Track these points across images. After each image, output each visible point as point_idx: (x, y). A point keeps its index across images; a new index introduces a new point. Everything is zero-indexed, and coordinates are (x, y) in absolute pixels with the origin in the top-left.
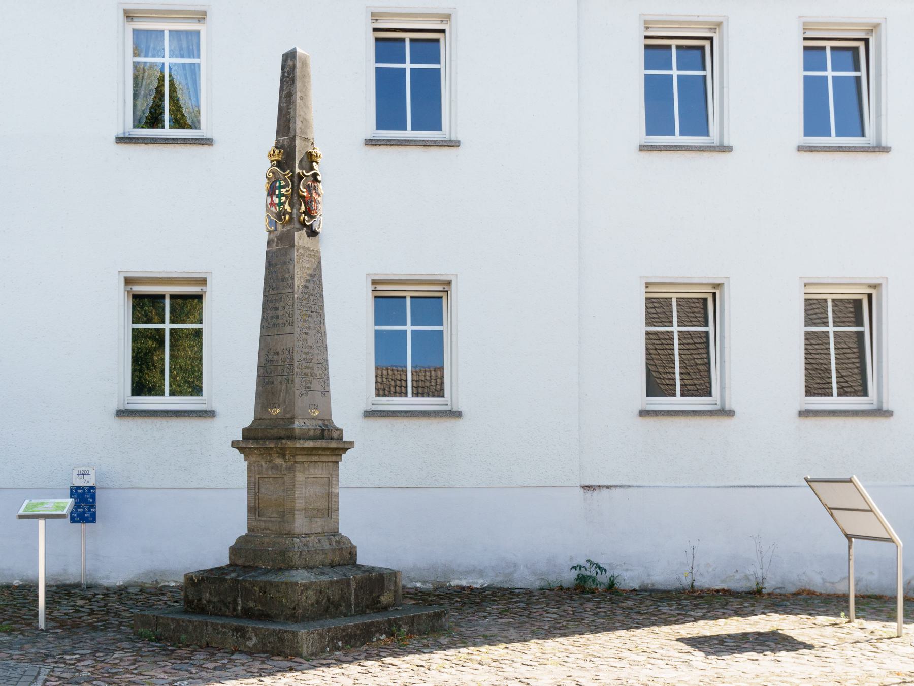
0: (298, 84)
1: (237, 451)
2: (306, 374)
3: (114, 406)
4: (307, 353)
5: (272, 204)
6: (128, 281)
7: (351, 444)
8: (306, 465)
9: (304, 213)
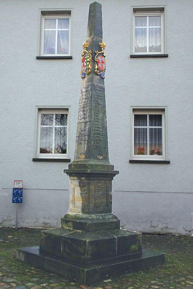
0: (150, 134)
1: (66, 174)
3: (33, 156)
4: (98, 130)
7: (117, 172)
9: (97, 69)
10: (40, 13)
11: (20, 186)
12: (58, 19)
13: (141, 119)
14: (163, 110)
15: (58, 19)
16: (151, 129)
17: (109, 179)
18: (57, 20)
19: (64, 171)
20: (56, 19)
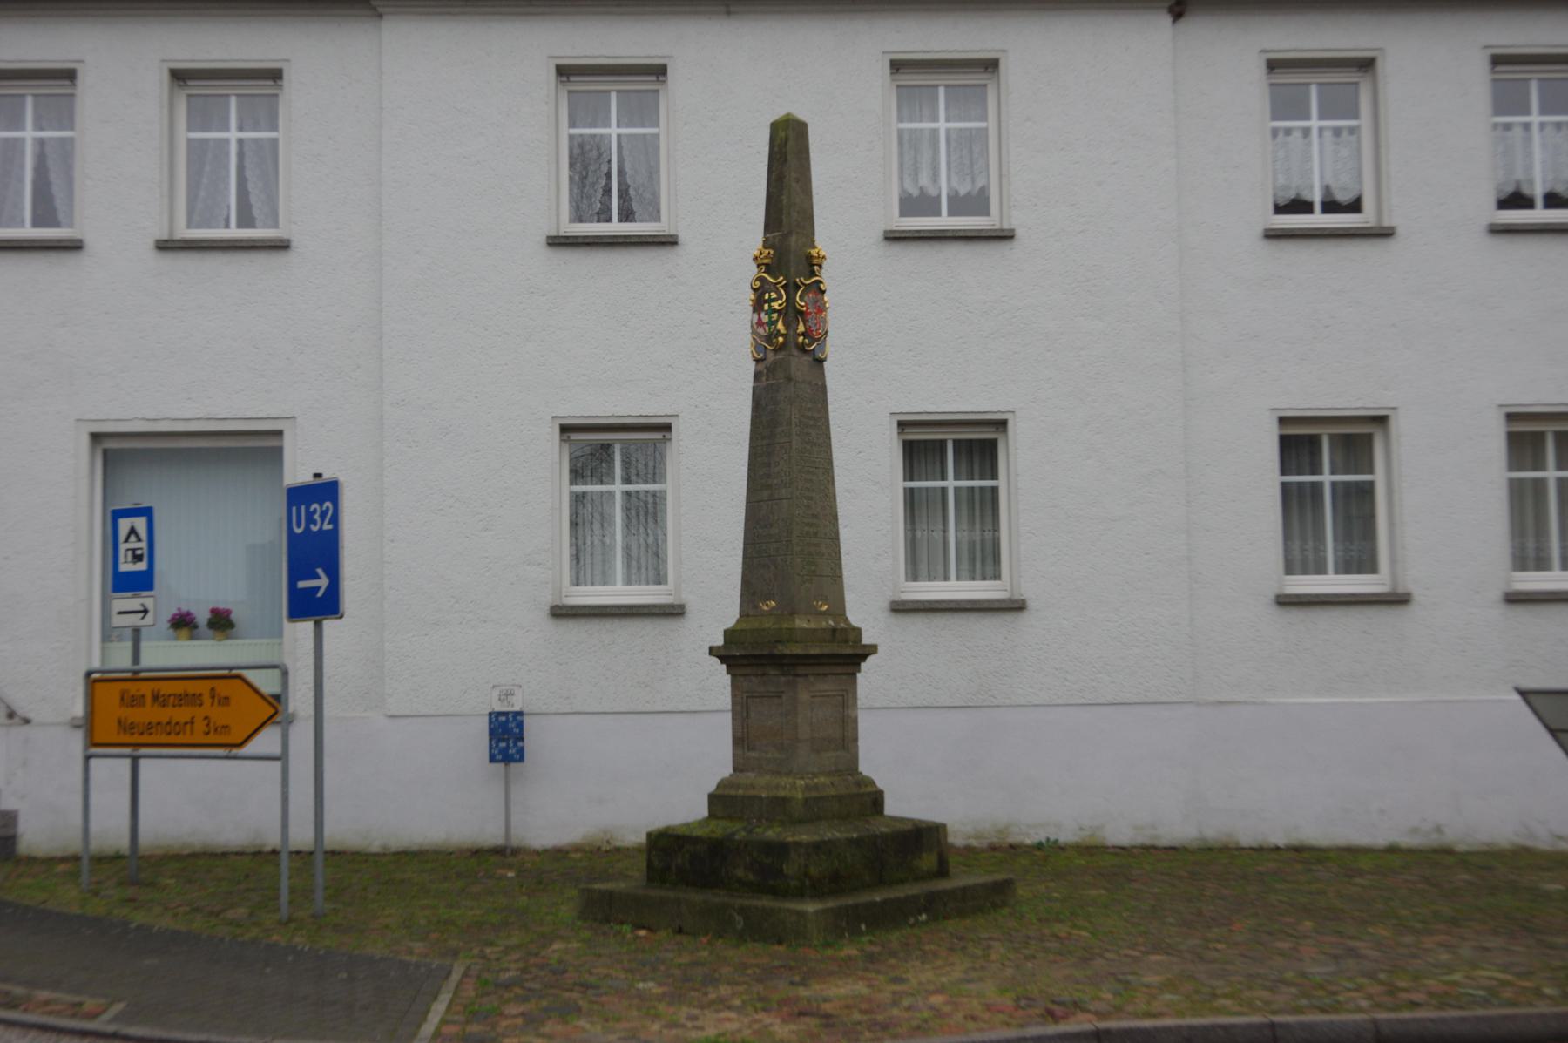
5: (760, 323)
7: (873, 649)
8: (812, 678)
10: (166, 76)
14: (1001, 425)
15: (947, 86)
17: (850, 669)
18: (942, 90)
20: (1308, 84)
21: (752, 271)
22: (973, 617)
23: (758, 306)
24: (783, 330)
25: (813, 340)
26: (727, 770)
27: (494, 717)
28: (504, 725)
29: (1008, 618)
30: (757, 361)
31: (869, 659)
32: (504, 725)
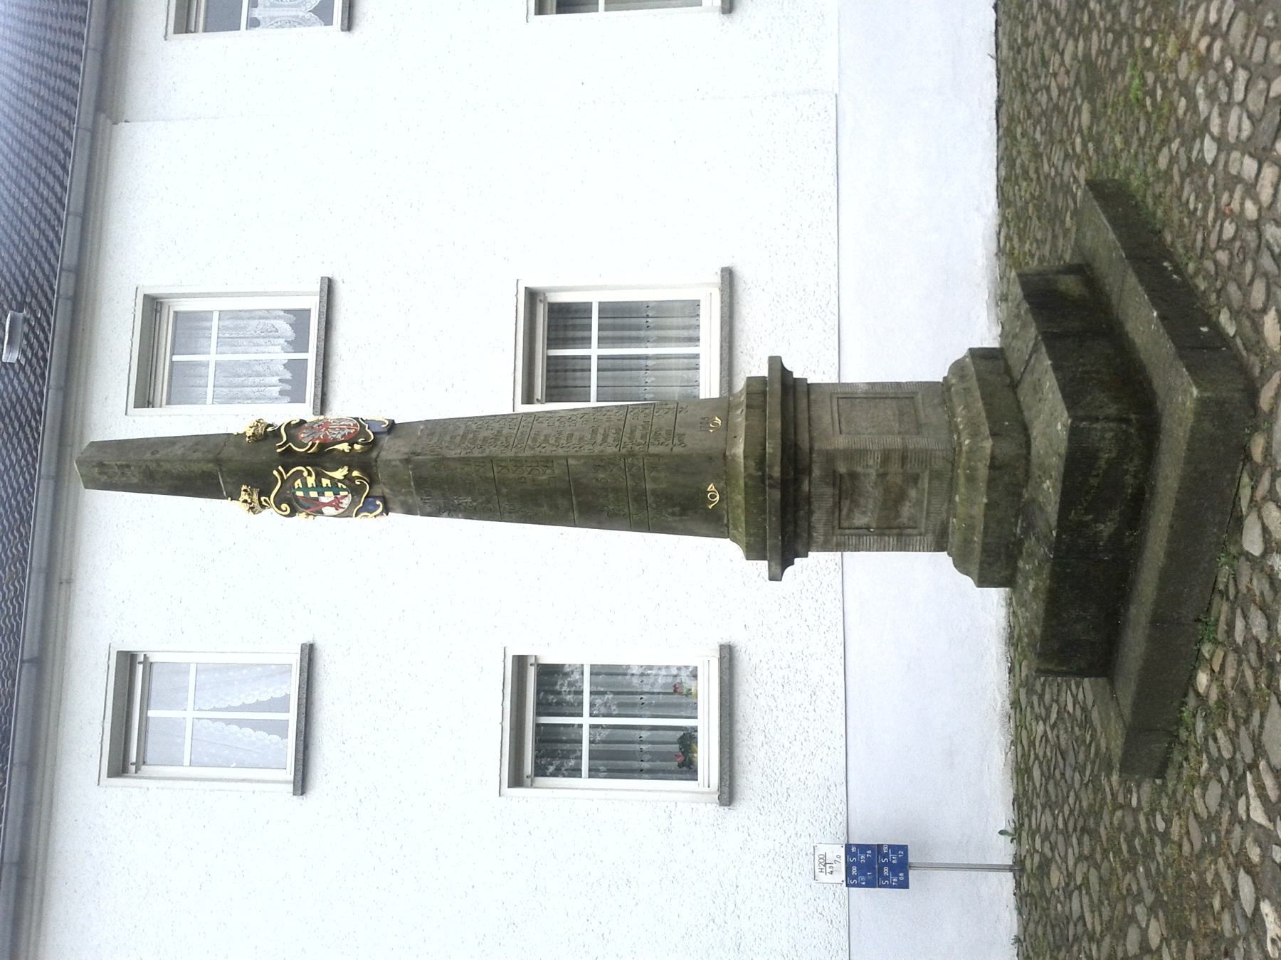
1: (789, 570)
2: (643, 437)
3: (712, 809)
5: (336, 504)
6: (517, 780)
7: (775, 362)
9: (351, 445)
11: (837, 852)
12: (173, 354)
13: (565, 379)
14: (532, 296)
15: (173, 354)
16: (601, 340)
19: (772, 578)
21: (271, 516)
22: (739, 325)
23: (315, 509)
24: (344, 471)
25: (362, 433)
26: (944, 559)
27: (852, 880)
28: (863, 868)
29: (741, 288)
30: (387, 510)
31: (788, 367)
32: (863, 868)
